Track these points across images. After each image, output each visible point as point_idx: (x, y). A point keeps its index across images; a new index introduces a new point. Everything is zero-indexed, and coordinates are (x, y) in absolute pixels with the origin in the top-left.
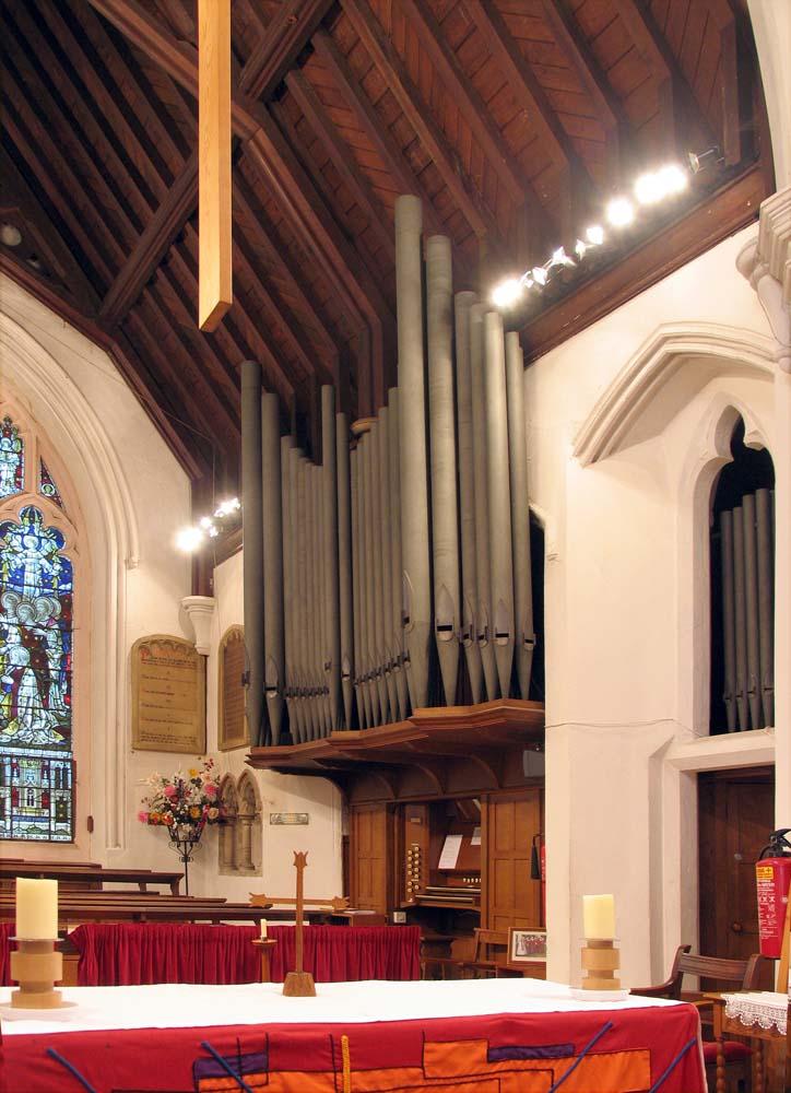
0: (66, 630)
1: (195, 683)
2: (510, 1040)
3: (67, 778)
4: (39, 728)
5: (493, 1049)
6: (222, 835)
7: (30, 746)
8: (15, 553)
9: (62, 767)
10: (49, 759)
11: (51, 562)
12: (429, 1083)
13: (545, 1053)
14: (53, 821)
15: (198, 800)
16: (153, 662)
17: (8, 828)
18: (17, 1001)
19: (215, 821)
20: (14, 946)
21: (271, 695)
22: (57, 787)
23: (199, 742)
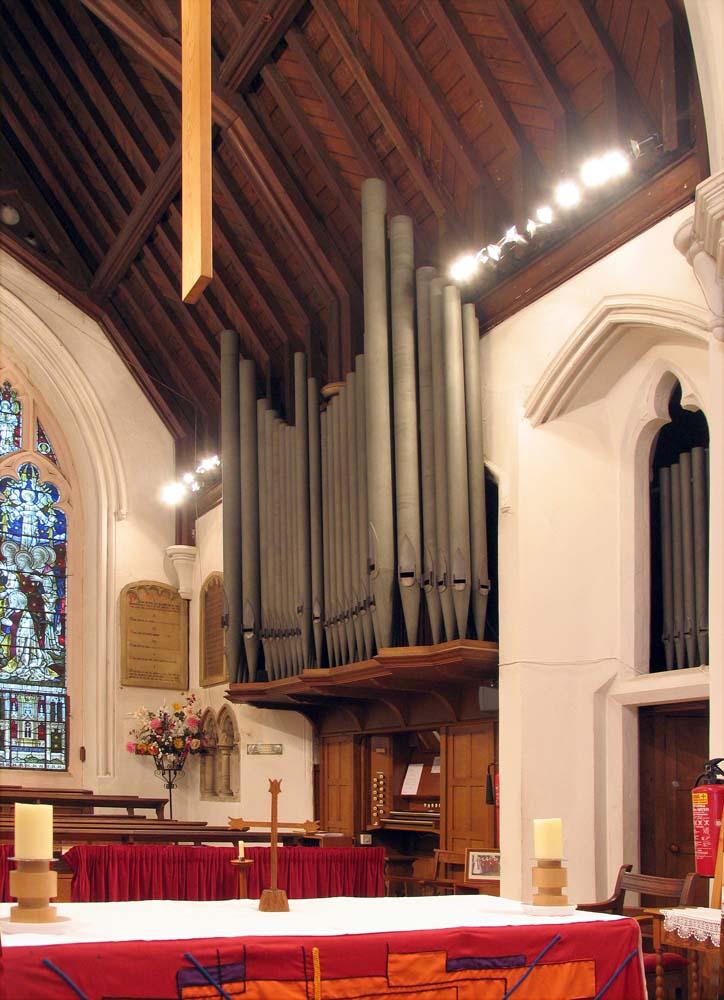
0: (60, 577)
1: (179, 625)
2: (467, 952)
3: (61, 712)
4: (35, 666)
5: (451, 960)
6: (204, 764)
7: (28, 683)
8: (14, 506)
9: (56, 702)
10: (45, 695)
11: (47, 514)
12: (393, 990)
13: (499, 963)
14: (48, 752)
15: (181, 732)
16: (140, 605)
17: (8, 757)
18: (15, 916)
19: (197, 751)
20: (13, 865)
21: (248, 636)
22: (52, 720)
23: (182, 679)
